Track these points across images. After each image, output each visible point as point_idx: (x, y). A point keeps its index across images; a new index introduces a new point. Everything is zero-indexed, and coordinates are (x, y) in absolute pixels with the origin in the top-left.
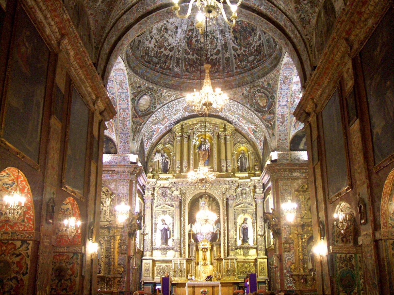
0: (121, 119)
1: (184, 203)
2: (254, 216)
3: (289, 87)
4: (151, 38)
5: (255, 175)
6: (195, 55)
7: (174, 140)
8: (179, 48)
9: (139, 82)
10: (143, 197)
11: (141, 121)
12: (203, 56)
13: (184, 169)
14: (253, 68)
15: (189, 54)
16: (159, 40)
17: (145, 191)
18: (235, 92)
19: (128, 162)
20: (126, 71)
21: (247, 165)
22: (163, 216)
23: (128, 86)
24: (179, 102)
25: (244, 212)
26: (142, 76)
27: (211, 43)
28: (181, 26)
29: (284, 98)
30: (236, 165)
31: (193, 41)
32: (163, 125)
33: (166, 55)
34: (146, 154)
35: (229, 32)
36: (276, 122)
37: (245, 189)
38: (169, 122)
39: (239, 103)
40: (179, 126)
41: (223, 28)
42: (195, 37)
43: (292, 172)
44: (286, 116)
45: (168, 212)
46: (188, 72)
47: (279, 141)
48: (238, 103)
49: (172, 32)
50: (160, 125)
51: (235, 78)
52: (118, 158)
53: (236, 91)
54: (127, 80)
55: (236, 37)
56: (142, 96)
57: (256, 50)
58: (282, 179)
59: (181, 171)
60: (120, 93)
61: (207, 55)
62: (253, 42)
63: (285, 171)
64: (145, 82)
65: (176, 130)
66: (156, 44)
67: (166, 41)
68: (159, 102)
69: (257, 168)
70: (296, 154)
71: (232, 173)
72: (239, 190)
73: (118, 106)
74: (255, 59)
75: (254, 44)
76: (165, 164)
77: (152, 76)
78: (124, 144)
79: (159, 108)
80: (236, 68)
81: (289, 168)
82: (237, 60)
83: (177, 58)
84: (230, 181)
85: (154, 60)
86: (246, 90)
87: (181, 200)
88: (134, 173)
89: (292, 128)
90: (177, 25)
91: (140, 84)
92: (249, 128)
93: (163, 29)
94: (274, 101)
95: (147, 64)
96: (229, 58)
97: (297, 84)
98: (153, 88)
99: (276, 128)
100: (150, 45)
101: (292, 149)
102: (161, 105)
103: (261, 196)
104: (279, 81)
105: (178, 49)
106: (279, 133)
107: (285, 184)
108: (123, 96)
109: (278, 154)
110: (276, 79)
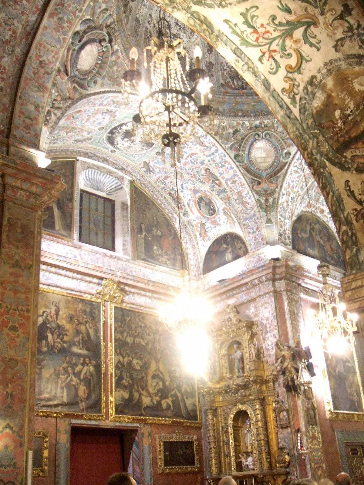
0: (236, 197)
11: (272, 187)
19: (266, 261)
56: (252, 144)
60: (210, 156)
73: (220, 178)
77: (253, 106)
78: (254, 235)
91: (233, 127)
95: (240, 91)
108: (218, 160)
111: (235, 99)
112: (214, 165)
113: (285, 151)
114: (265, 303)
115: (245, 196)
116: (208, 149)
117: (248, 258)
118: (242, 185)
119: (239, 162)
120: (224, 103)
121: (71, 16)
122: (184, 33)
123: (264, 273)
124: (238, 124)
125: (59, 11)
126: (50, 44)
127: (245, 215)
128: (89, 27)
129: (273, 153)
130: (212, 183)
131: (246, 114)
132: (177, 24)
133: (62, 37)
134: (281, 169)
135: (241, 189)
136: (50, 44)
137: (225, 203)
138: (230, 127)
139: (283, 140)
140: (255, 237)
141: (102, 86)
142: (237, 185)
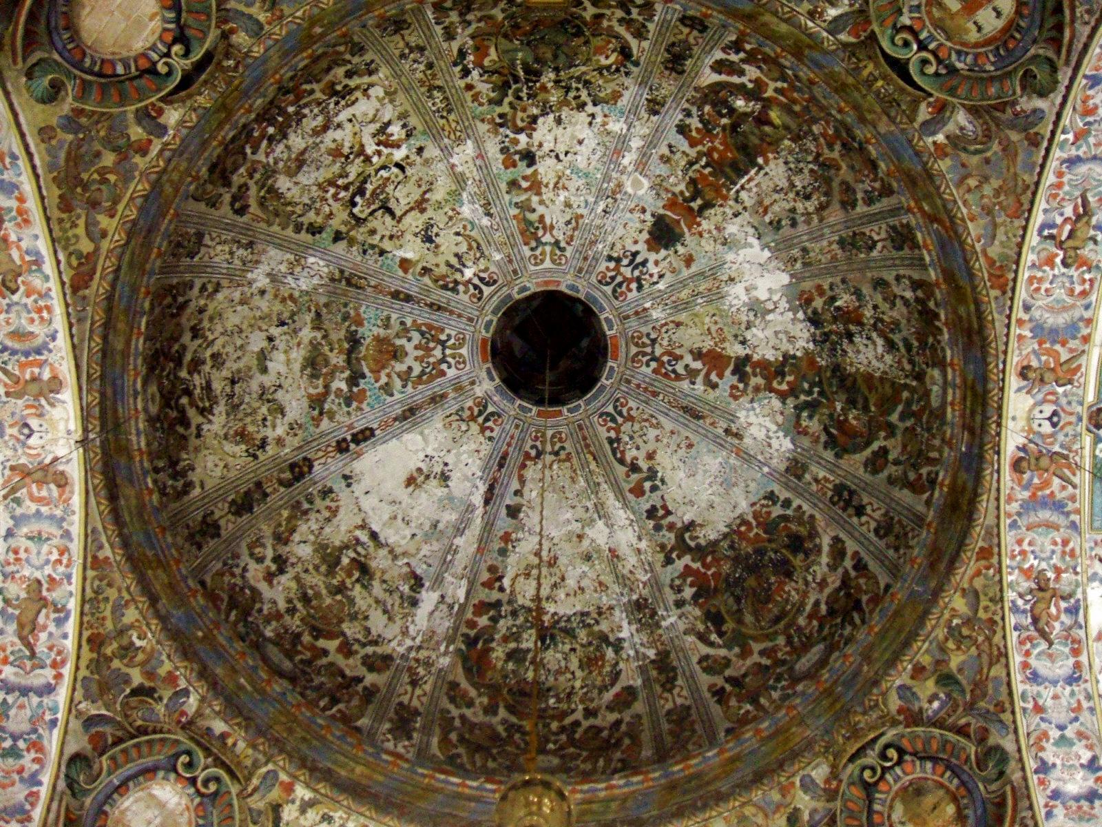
3: (1077, 665)
6: (502, 712)
8: (421, 671)
9: (151, 655)
15: (470, 704)
16: (318, 595)
20: (77, 500)
27: (590, 663)
28: (438, 581)
33: (343, 676)
35: (679, 604)
41: (645, 592)
53: (749, 810)
54: (75, 586)
55: (716, 619)
56: (149, 772)
57: (832, 612)
66: (299, 606)
67: (354, 617)
83: (401, 704)
86: (807, 785)
90: (419, 571)
93: (345, 561)
104: (1012, 620)
116: (28, 664)
120: (182, 602)
124: (171, 679)
138: (142, 664)
141: (45, 133)
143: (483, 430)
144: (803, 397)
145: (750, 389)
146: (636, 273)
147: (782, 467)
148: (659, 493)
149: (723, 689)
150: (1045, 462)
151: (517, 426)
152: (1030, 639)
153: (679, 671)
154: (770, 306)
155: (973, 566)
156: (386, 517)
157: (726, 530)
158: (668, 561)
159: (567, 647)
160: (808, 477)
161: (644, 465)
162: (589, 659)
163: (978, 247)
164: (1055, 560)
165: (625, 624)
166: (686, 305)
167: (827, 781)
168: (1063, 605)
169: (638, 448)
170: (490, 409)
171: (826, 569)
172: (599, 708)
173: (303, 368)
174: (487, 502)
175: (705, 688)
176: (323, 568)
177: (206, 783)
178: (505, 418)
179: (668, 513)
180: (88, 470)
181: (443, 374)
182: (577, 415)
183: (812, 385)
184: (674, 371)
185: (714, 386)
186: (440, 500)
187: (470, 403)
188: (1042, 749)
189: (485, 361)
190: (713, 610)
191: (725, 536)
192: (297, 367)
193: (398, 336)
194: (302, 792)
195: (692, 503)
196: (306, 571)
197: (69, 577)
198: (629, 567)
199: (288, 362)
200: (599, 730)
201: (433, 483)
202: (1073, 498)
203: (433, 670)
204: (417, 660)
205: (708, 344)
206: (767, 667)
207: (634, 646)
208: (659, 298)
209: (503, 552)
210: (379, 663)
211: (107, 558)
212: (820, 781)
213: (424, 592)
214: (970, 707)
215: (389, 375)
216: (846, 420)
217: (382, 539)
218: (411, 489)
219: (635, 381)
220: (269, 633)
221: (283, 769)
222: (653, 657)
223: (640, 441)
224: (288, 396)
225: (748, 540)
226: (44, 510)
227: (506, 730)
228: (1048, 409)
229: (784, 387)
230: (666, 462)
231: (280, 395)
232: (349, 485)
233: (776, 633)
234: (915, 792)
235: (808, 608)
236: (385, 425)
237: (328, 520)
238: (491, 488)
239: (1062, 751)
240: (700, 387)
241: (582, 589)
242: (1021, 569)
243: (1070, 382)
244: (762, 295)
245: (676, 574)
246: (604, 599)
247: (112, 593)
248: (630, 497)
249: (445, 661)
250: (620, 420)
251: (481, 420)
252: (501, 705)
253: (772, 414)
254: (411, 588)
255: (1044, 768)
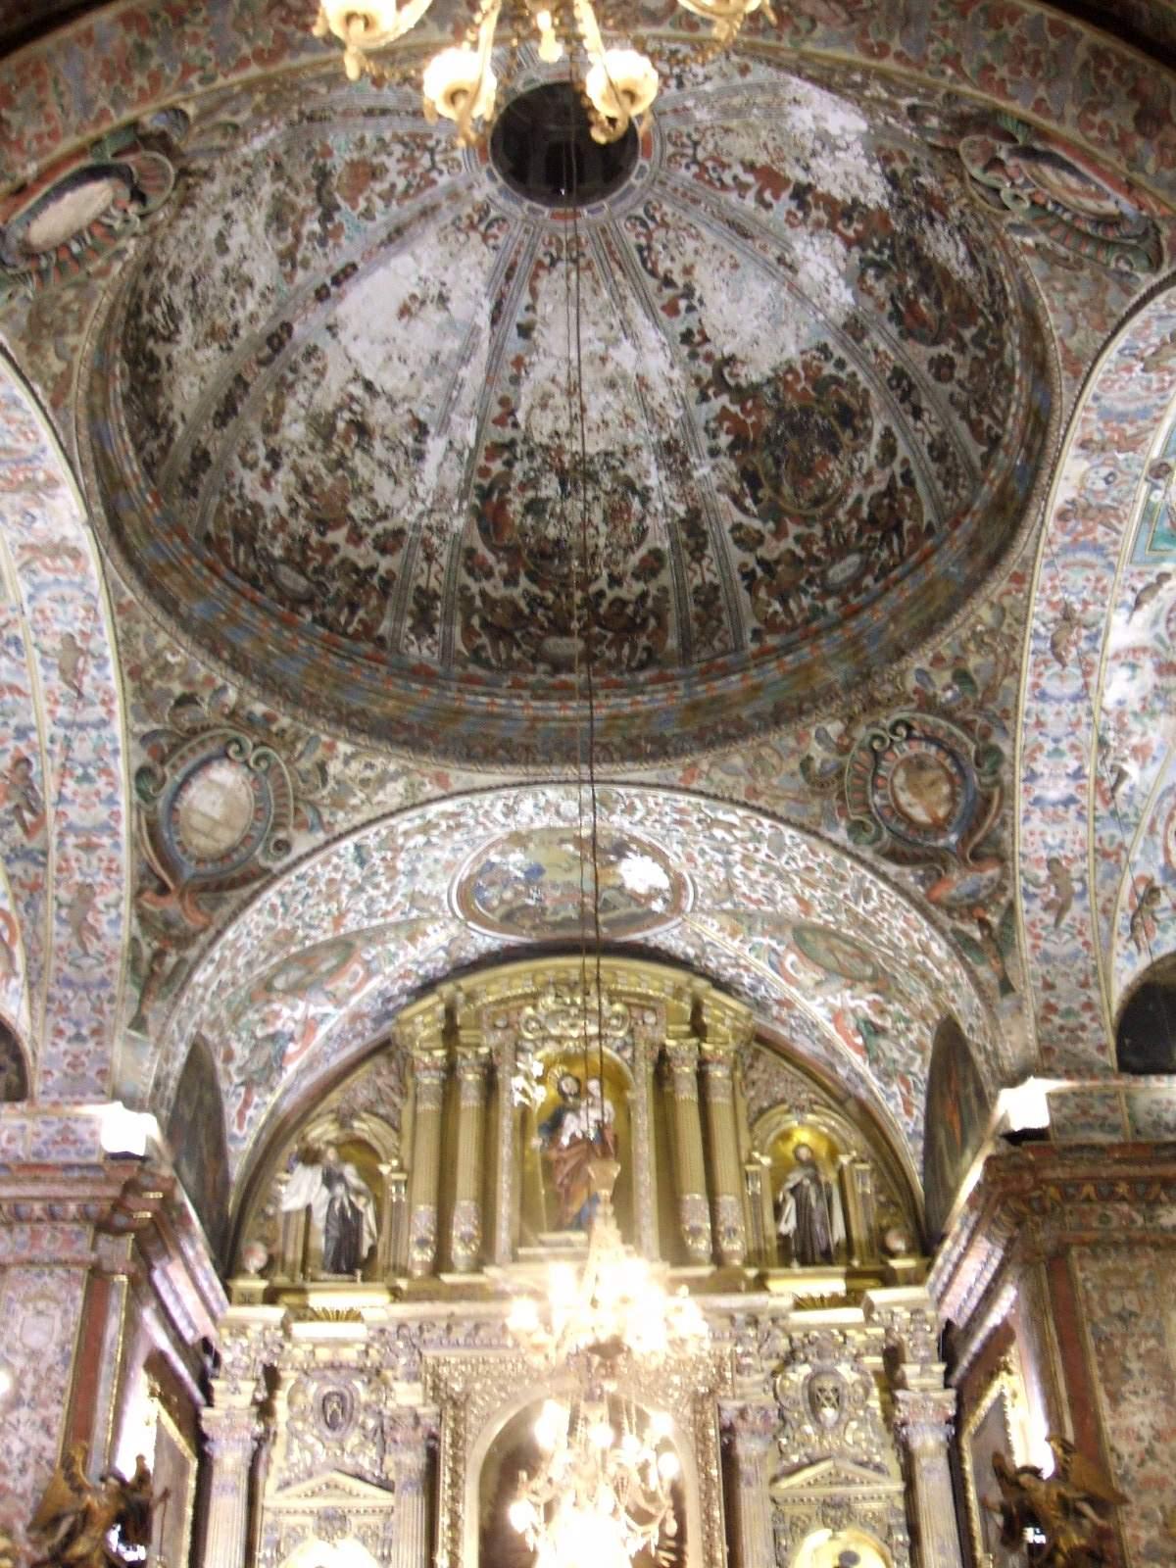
0: (65, 895)
1: (455, 1459)
2: (901, 1537)
3: (1086, 686)
4: (274, 456)
5: (888, 1279)
6: (524, 582)
7: (403, 1094)
8: (435, 541)
9: (186, 667)
10: (197, 1417)
11: (191, 923)
12: (564, 585)
13: (460, 1252)
14: (855, 612)
15: (489, 574)
16: (318, 479)
17: (216, 1384)
18: (759, 758)
19: (90, 1152)
20: (94, 568)
21: (839, 1233)
22: (324, 1545)
23: (112, 676)
24: (427, 828)
25: (836, 1512)
26: (210, 640)
27: (614, 515)
28: (445, 424)
29: (1057, 752)
30: (771, 1232)
31: (510, 508)
32: (339, 1003)
33: (356, 569)
34: (237, 1169)
35: (714, 452)
36: (1022, 904)
37: (835, 1374)
38: (375, 984)
39: (787, 822)
40: (430, 1009)
41: (677, 432)
42: (523, 487)
43: (1154, 1203)
44: (1075, 870)
45: (354, 1521)
46: (485, 664)
47: (1045, 1019)
48: (781, 820)
49: (392, 449)
50: (322, 998)
51: (755, 676)
52: (31, 1126)
53: (765, 751)
54: (108, 635)
55: (751, 478)
56: (205, 763)
57: (873, 520)
58: (1098, 1247)
59: (441, 1263)
60: (69, 725)
61: (586, 581)
62: (848, 482)
63: (1109, 1195)
64: (220, 675)
65: (412, 1040)
66: (301, 500)
67: (358, 492)
68: (308, 814)
69: (897, 1243)
70: (1163, 1096)
71: (752, 1273)
72: (801, 1373)
73: (51, 812)
74: (866, 567)
75: (855, 491)
76: (347, 1226)
77: (269, 654)
78: (76, 1048)
79: (308, 855)
80: (757, 635)
81: (1133, 1170)
82: (762, 594)
83: (419, 588)
84: (740, 1317)
85: (289, 583)
86: (822, 737)
87: (434, 1437)
88: (120, 1220)
89: (1118, 945)
90: (422, 417)
91: (190, 683)
92: (837, 1017)
93: (341, 425)
94: (998, 782)
96: (715, 588)
97: (1133, 667)
98: (269, 719)
99: (1025, 941)
100: (265, 499)
101: (1134, 1060)
102: (321, 836)
103: (939, 1405)
104: (1030, 644)
105: (426, 543)
106: (1041, 970)
107: (1115, 1281)
109: (1050, 1096)
110: (1004, 639)
111: (237, 604)
112: (58, 760)
113: (281, 835)
114: (42, 1296)
115: (101, 907)
117: (23, 1114)
118: (110, 870)
119: (141, 792)
120: (201, 594)
121: (174, 68)
122: (194, 321)
123: (86, 1191)
124: (209, 681)
125: (158, 25)
126: (61, 95)
127: (67, 969)
128: (163, 136)
129: (241, 822)
130: (7, 812)
131: (239, 664)
132: (194, 284)
133: (103, 102)
134: (245, 880)
135: (101, 878)
136: (61, 95)
137: (16, 897)
138: (180, 676)
139: (296, 799)
140: (76, 1057)
142: (95, 862)
143: (485, 238)
144: (870, 253)
145: (810, 222)
146: (676, 70)
147: (841, 320)
148: (695, 316)
149: (753, 572)
150: (1092, 513)
151: (527, 231)
152: (1045, 662)
153: (710, 537)
154: (843, 144)
155: (1005, 585)
156: (379, 360)
157: (770, 374)
158: (704, 398)
159: (590, 495)
160: (866, 343)
161: (679, 279)
162: (614, 510)
163: (1056, 333)
164: (1085, 595)
165: (653, 469)
166: (739, 113)
167: (840, 737)
168: (1084, 632)
169: (673, 259)
170: (493, 213)
171: (873, 461)
172: (625, 574)
173: (268, 225)
174: (494, 321)
175: (735, 566)
176: (319, 444)
177: (257, 762)
178: (511, 223)
179: (706, 340)
180: (97, 536)
181: (433, 182)
182: (600, 217)
183: (883, 244)
184: (720, 180)
185: (768, 206)
186: (440, 327)
187: (468, 210)
188: (1034, 759)
189: (484, 159)
190: (750, 468)
191: (769, 381)
192: (260, 229)
193: (375, 153)
194: (344, 748)
195: (733, 333)
196: (302, 454)
197: (100, 631)
198: (659, 399)
199: (250, 228)
200: (624, 603)
201: (430, 308)
202: (1115, 543)
203: (448, 537)
204: (429, 528)
205: (762, 159)
206: (800, 561)
207: (662, 498)
208: (704, 100)
209: (515, 380)
210: (391, 542)
211: (131, 603)
212: (834, 736)
213: (429, 440)
214: (980, 707)
215: (368, 200)
216: (916, 301)
217: (378, 387)
218: (405, 320)
219: (670, 184)
220: (277, 552)
221: (325, 732)
222: (682, 514)
223: (675, 253)
224: (254, 265)
225: (795, 392)
226: (62, 577)
227: (529, 605)
228: (1105, 471)
229: (851, 233)
230: (706, 279)
231: (246, 268)
232: (334, 336)
233: (813, 518)
234: (917, 765)
235: (850, 501)
236: (368, 255)
237: (316, 385)
238: (498, 307)
239: (1051, 762)
240: (750, 202)
241: (605, 423)
242: (1049, 603)
243: (1134, 450)
244: (834, 130)
245: (712, 415)
246: (631, 436)
247: (141, 628)
248: (662, 315)
249: (459, 524)
250: (652, 225)
251: (482, 227)
252: (522, 572)
253: (833, 257)
254: (416, 439)
255: (1033, 776)
